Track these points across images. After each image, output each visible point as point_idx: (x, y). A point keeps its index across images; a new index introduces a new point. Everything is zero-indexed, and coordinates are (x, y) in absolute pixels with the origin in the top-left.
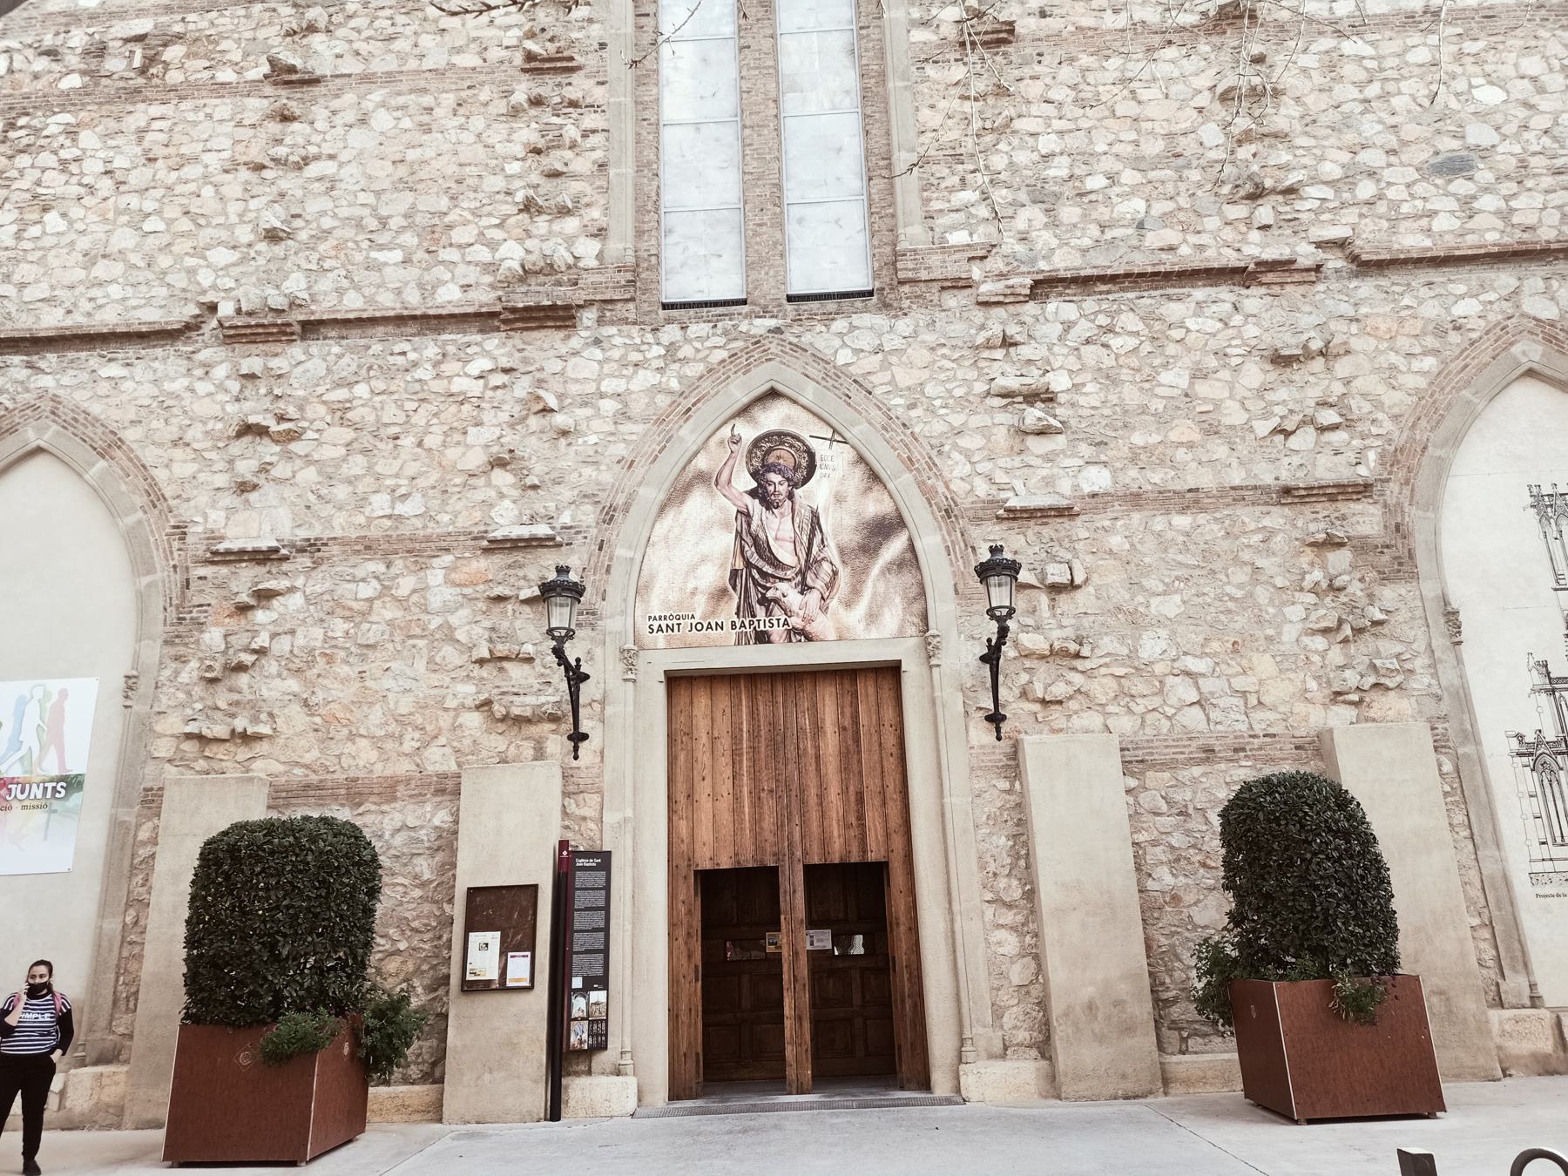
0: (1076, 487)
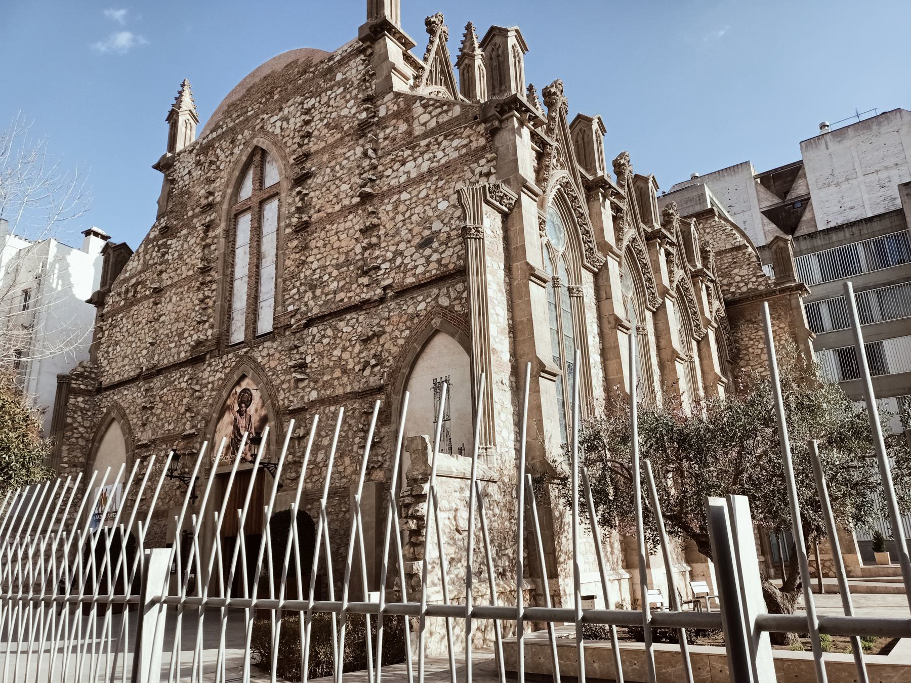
0: (309, 399)
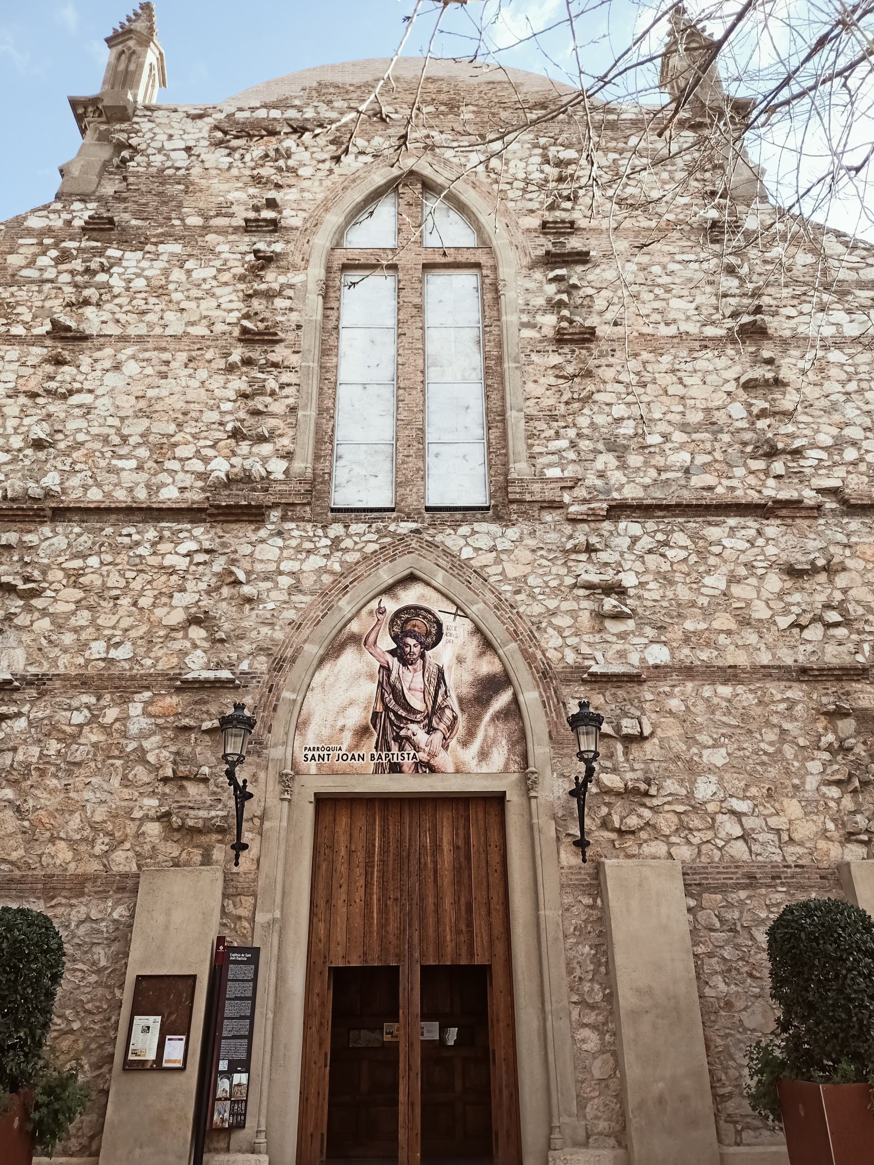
0: (643, 660)
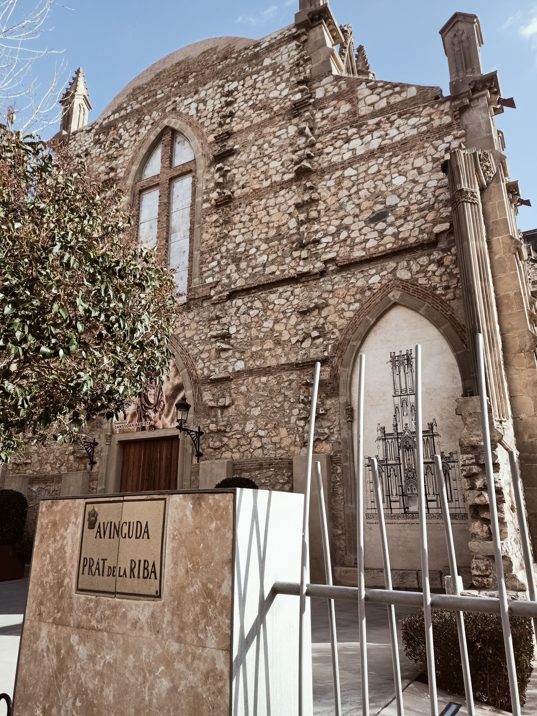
0: (234, 369)
